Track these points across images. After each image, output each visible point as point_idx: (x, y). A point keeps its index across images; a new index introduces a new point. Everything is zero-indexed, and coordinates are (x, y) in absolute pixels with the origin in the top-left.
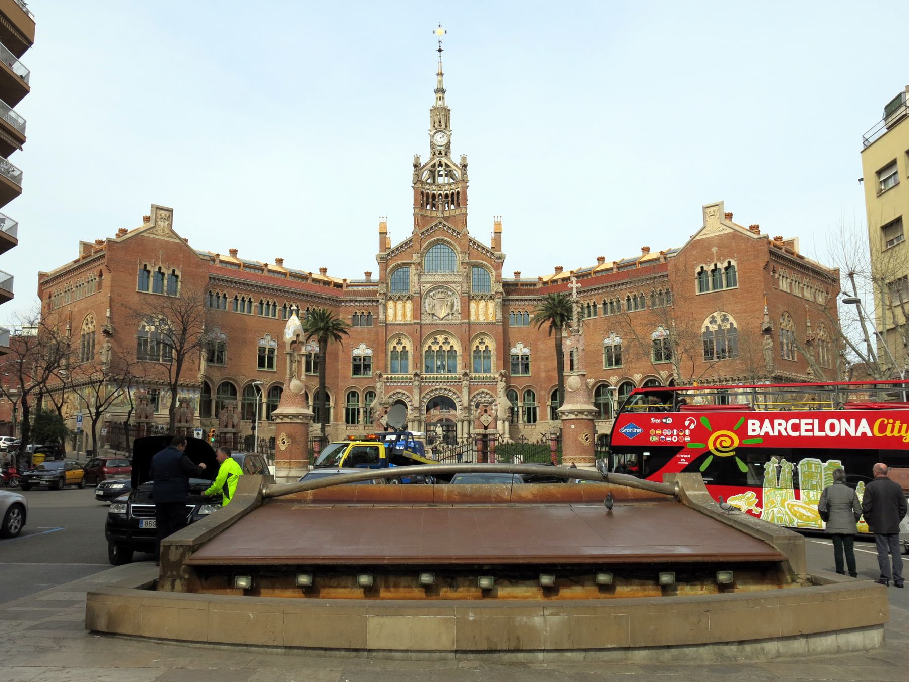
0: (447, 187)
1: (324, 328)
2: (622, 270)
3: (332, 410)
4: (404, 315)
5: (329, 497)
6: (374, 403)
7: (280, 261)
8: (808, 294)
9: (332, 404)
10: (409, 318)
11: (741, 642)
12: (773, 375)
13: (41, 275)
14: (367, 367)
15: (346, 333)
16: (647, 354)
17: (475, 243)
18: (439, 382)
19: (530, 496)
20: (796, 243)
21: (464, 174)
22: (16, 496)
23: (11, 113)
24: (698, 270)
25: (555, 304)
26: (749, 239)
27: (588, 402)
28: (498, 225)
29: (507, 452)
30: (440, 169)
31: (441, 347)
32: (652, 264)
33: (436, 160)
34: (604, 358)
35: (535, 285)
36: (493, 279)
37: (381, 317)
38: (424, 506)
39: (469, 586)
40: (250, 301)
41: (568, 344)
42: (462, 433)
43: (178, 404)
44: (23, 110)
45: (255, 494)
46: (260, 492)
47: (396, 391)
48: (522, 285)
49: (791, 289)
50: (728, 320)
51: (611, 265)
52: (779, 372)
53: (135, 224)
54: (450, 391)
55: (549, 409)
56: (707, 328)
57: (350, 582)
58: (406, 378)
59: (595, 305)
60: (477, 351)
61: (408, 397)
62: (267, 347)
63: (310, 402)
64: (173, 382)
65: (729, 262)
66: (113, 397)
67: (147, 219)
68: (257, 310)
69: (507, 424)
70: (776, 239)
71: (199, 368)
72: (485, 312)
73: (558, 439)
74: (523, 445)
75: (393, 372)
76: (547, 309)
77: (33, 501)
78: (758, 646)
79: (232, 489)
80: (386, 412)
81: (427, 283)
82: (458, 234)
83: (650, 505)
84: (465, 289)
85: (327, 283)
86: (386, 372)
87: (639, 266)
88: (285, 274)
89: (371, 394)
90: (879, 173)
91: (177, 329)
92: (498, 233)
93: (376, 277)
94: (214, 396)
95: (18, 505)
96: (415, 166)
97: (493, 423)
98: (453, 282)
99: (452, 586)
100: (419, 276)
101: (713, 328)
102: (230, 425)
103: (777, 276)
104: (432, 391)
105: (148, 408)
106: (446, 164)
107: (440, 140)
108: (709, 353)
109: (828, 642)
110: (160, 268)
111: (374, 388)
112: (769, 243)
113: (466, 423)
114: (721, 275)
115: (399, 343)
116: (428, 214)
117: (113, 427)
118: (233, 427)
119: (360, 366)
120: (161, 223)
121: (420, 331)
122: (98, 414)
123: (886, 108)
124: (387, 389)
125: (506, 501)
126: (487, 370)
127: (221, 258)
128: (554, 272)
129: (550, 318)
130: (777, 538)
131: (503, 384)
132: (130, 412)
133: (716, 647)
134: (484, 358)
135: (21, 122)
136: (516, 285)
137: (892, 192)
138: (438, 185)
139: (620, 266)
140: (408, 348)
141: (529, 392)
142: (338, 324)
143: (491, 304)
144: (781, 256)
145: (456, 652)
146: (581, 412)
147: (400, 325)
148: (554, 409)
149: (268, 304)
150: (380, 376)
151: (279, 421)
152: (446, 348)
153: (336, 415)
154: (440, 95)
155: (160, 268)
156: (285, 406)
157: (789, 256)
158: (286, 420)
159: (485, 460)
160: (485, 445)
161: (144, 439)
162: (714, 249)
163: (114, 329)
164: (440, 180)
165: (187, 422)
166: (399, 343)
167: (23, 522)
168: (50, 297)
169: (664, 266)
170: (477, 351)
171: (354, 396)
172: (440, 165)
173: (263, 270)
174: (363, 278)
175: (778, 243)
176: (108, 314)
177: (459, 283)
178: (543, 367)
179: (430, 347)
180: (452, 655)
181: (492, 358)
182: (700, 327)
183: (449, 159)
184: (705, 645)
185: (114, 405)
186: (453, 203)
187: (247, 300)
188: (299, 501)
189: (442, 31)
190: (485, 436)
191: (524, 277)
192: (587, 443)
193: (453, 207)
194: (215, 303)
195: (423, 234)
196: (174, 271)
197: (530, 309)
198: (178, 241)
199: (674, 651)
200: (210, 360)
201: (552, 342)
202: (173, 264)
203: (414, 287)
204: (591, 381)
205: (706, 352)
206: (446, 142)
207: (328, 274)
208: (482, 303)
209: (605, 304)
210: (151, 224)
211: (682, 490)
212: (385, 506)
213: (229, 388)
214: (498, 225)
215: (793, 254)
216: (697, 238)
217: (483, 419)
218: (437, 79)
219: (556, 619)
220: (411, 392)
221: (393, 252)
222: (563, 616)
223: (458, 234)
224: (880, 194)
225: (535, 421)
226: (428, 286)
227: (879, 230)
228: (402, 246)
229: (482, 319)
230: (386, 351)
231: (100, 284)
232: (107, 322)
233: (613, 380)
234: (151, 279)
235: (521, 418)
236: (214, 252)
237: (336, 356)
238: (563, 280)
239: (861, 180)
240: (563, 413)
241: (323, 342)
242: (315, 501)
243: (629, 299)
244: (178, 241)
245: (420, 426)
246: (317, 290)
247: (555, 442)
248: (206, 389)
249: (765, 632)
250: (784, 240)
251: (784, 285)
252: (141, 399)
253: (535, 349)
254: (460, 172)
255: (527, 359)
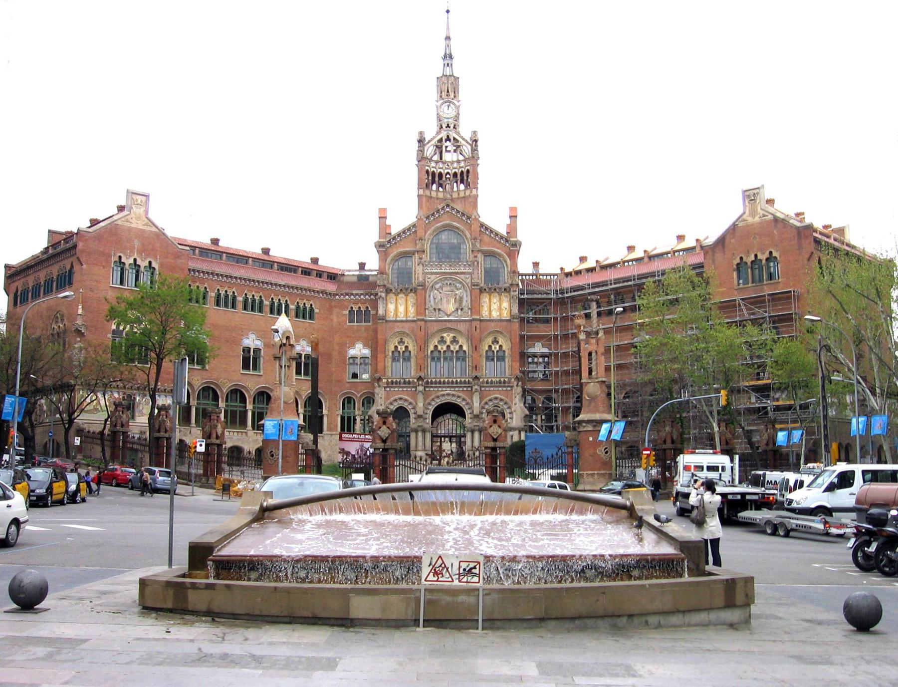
0: (455, 165)
3: (325, 419)
6: (372, 411)
9: (325, 412)
10: (412, 315)
13: (7, 267)
20: (846, 231)
21: (474, 149)
30: (448, 143)
31: (448, 347)
33: (443, 135)
42: (472, 442)
43: (156, 411)
45: (258, 508)
46: (261, 505)
47: (397, 397)
54: (459, 397)
61: (410, 403)
62: (252, 347)
63: (301, 410)
66: (85, 404)
79: (554, 472)
81: (432, 274)
82: (469, 218)
92: (513, 217)
96: (419, 141)
102: (214, 436)
104: (438, 397)
105: (124, 416)
106: (454, 139)
111: (373, 394)
116: (434, 194)
121: (422, 328)
132: (106, 420)
138: (444, 163)
140: (411, 348)
147: (402, 321)
152: (455, 348)
154: (448, 61)
155: (135, 260)
164: (447, 157)
171: (349, 402)
172: (448, 139)
177: (469, 273)
181: (507, 360)
185: (86, 412)
186: (462, 182)
193: (462, 187)
196: (150, 263)
198: (154, 229)
202: (148, 255)
206: (455, 114)
221: (394, 238)
223: (469, 218)
226: (433, 277)
228: (404, 232)
244: (154, 229)
252: (117, 405)
254: (469, 147)
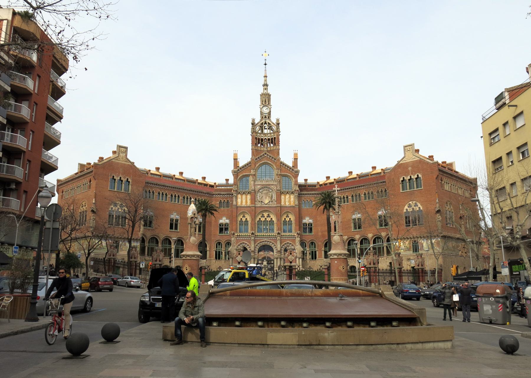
1: (205, 209)
2: (361, 178)
3: (208, 252)
4: (246, 202)
5: (236, 293)
7: (181, 173)
8: (460, 192)
9: (208, 249)
10: (249, 203)
11: (398, 344)
12: (442, 235)
14: (226, 229)
15: (216, 210)
16: (375, 224)
17: (283, 164)
18: (265, 236)
19: (320, 294)
20: (453, 164)
21: (278, 128)
22: (89, 294)
23: (55, 103)
24: (402, 179)
25: (326, 196)
26: (428, 163)
27: (344, 249)
28: (296, 155)
29: (302, 275)
30: (265, 125)
31: (266, 219)
32: (378, 175)
33: (263, 121)
34: (352, 225)
35: (315, 186)
36: (293, 183)
37: (234, 203)
38: (277, 298)
39: (299, 327)
40: (166, 195)
41: (333, 218)
42: (277, 264)
44: (61, 102)
45: (208, 292)
48: (309, 186)
49: (451, 189)
50: (417, 206)
51: (356, 176)
52: (445, 234)
53: (107, 155)
55: (323, 252)
56: (407, 209)
57: (254, 324)
58: (247, 235)
59: (347, 197)
60: (285, 221)
61: (248, 245)
62: (175, 219)
64: (130, 238)
65: (418, 175)
67: (114, 152)
68: (170, 199)
69: (301, 260)
70: (443, 163)
71: (141, 230)
72: (289, 200)
73: (329, 268)
74: (310, 272)
75: (240, 232)
76: (323, 200)
77: (97, 297)
78: (404, 345)
80: (239, 254)
81: (259, 185)
82: (275, 159)
83: (369, 298)
84: (278, 188)
85: (206, 185)
86: (237, 232)
87: (370, 177)
88: (184, 180)
89: (228, 244)
90: (490, 134)
91: (133, 210)
92: (296, 159)
93: (231, 181)
94: (147, 244)
95: (90, 298)
96: (252, 124)
97: (294, 261)
98: (272, 185)
99: (293, 326)
100: (255, 181)
101: (410, 210)
103: (443, 182)
105: (114, 251)
107: (265, 110)
108: (408, 223)
109: (431, 345)
110: (120, 178)
111: (230, 241)
112: (439, 165)
113: (279, 259)
114: (413, 182)
115: (244, 217)
117: (95, 260)
118: (160, 261)
119: (223, 229)
120: (121, 155)
121: (254, 211)
122: (89, 254)
123: (495, 99)
124: (237, 241)
125: (310, 296)
126: (290, 231)
127: (151, 172)
128: (326, 179)
129: (323, 204)
130: (415, 309)
131: (299, 239)
133: (389, 345)
134: (289, 224)
135: (61, 108)
136: (306, 186)
137: (497, 144)
139: (360, 176)
140: (248, 219)
141: (312, 243)
142: (212, 207)
143: (292, 197)
144: (446, 172)
145: (298, 345)
146: (340, 255)
147: (244, 207)
148: (326, 252)
149: (175, 196)
150: (234, 234)
151: (184, 258)
153: (210, 254)
154: (265, 87)
155: (120, 178)
156: (187, 251)
157: (449, 172)
158: (188, 258)
159: (290, 279)
160: (290, 271)
161: (158, 269)
162: (410, 168)
163: (97, 209)
164: (265, 131)
165: (135, 258)
166: (244, 217)
167: (92, 306)
168: (63, 192)
169: (384, 177)
170: (285, 221)
171: (219, 245)
172: (266, 123)
173: (172, 178)
174: (224, 182)
175: (444, 165)
176: (94, 202)
177: (275, 185)
178: (320, 230)
179: (260, 219)
180: (297, 346)
182: (403, 209)
183: (270, 120)
184: (385, 344)
187: (164, 194)
188: (225, 296)
189: (264, 54)
190: (291, 267)
191: (309, 182)
192: (344, 271)
194: (151, 196)
195: (256, 159)
196: (128, 179)
197: (313, 199)
198: (130, 164)
199: (374, 346)
200: (145, 225)
201: (325, 217)
203: (251, 187)
204: (345, 238)
205: (406, 223)
207: (206, 180)
208: (288, 196)
209: (352, 196)
210: (116, 155)
211: (382, 292)
212: (260, 298)
213: (154, 240)
214: (296, 155)
215: (452, 170)
216: (401, 162)
217: (289, 258)
218: (263, 79)
219: (332, 334)
220: (250, 243)
221: (241, 169)
222: (335, 333)
223: (275, 159)
224: (491, 144)
225: (316, 258)
226: (259, 186)
227: (491, 163)
228: (245, 166)
229: (287, 204)
230: (237, 221)
231: (90, 186)
232: (93, 206)
233: (357, 237)
234: (116, 183)
235: (309, 257)
236: (148, 169)
237: (210, 223)
238: (331, 183)
239: (482, 137)
240: (331, 255)
241: (204, 216)
242: (231, 295)
243: (365, 194)
244: (130, 164)
245: (254, 261)
246: (200, 188)
247: (326, 270)
248: (143, 241)
249: (407, 340)
250: (447, 163)
251: (447, 187)
253: (315, 220)
255: (311, 225)
